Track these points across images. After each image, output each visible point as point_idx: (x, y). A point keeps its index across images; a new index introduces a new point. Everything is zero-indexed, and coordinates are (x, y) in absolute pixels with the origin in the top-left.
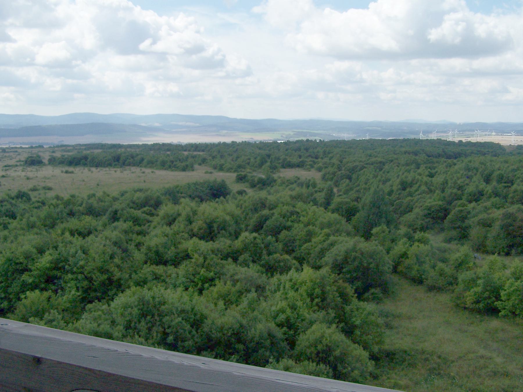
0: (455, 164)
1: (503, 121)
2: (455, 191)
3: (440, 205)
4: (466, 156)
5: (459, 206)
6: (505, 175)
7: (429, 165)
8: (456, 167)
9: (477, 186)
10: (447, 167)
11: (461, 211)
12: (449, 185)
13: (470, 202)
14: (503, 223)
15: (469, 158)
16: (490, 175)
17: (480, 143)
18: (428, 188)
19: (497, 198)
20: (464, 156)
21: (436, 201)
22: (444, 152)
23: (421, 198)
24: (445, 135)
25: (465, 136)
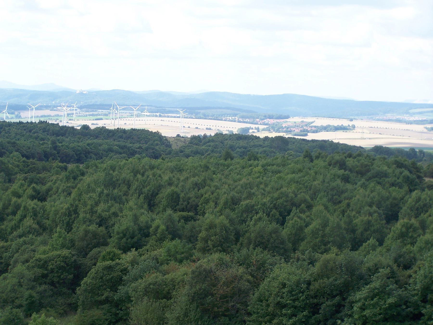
0: (83, 174)
1: (163, 89)
2: (93, 227)
3: (65, 257)
4: (99, 157)
5: (104, 259)
6: (182, 195)
7: (31, 175)
8: (87, 179)
9: (136, 218)
10: (68, 178)
11: (110, 268)
12: (81, 216)
13: (125, 250)
14: (194, 290)
15: (108, 163)
16: (154, 195)
17: (124, 131)
18: (38, 223)
19: (177, 241)
20: (93, 156)
21: (56, 249)
22: (55, 148)
23: (25, 243)
24: (53, 113)
25: (92, 117)
